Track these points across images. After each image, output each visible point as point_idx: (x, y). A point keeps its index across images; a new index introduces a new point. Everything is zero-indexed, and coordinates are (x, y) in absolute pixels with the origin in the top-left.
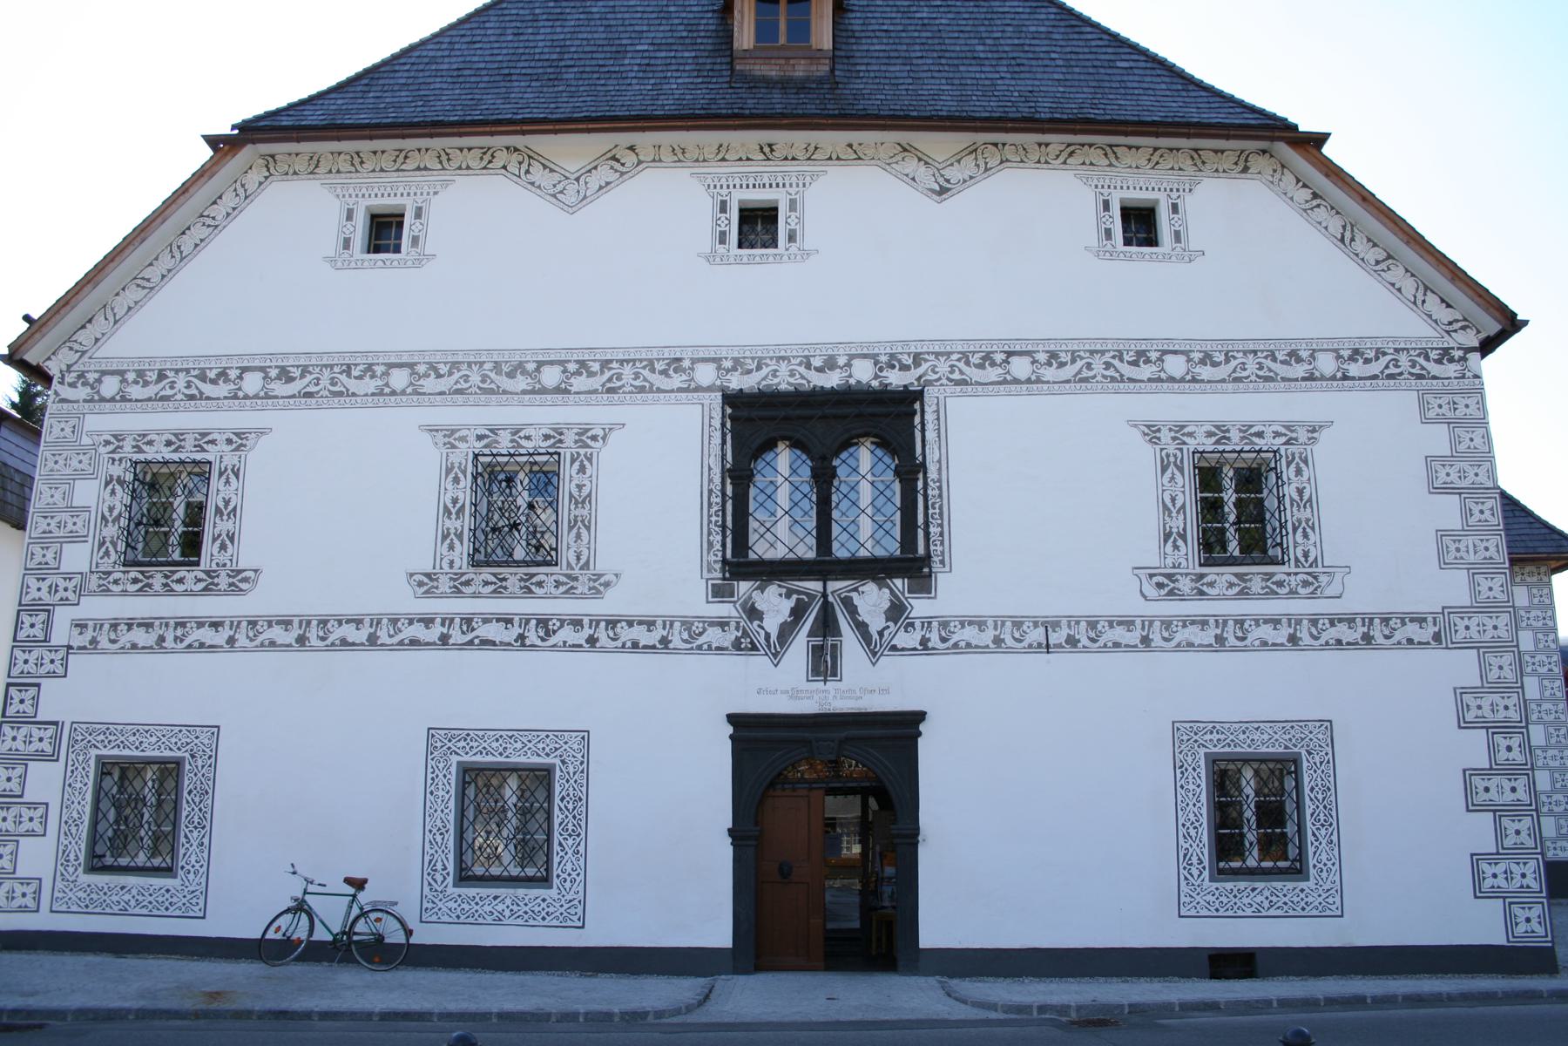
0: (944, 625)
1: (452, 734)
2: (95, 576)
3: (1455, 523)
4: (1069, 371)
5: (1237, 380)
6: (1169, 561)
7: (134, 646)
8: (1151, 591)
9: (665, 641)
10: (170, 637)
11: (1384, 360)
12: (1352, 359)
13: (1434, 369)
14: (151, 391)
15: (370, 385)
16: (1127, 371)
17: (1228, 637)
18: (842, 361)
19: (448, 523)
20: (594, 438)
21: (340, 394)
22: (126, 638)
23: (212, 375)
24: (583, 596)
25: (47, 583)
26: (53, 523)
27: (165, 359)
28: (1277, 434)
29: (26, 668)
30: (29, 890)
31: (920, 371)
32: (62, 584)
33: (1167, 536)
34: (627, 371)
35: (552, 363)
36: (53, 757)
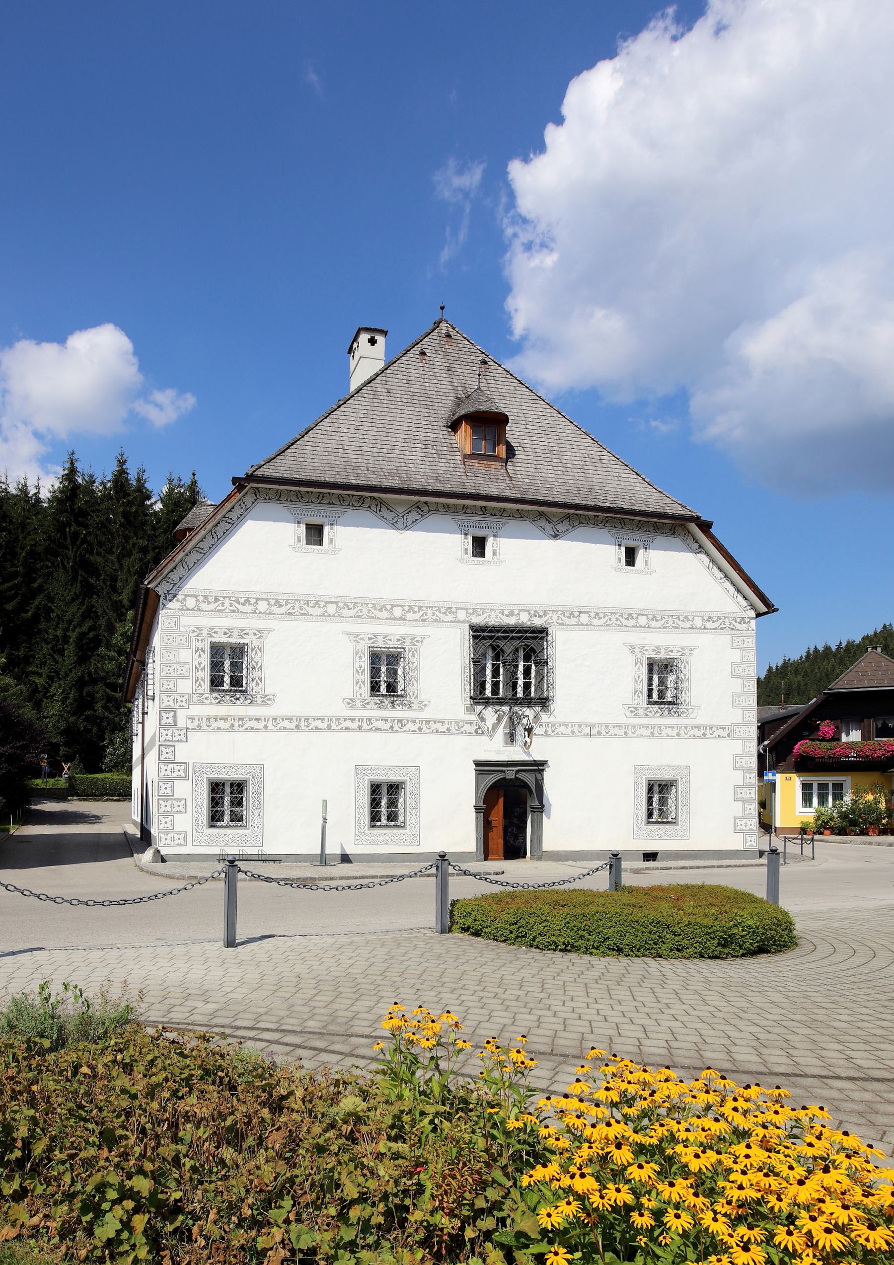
0: (553, 725)
1: (365, 768)
2: (195, 696)
3: (739, 690)
4: (602, 621)
5: (665, 628)
6: (636, 702)
7: (219, 729)
8: (628, 714)
9: (448, 730)
10: (236, 724)
11: (720, 621)
12: (708, 620)
13: (738, 626)
14: (212, 607)
15: (319, 611)
16: (624, 622)
17: (654, 733)
18: (516, 612)
19: (358, 677)
20: (417, 641)
21: (305, 614)
22: (214, 725)
23: (242, 601)
24: (415, 710)
25: (172, 698)
26: (171, 669)
27: (217, 591)
28: (678, 651)
29: (167, 738)
30: (181, 837)
31: (546, 618)
32: (179, 699)
33: (636, 692)
34: (429, 611)
35: (398, 606)
36: (186, 778)
